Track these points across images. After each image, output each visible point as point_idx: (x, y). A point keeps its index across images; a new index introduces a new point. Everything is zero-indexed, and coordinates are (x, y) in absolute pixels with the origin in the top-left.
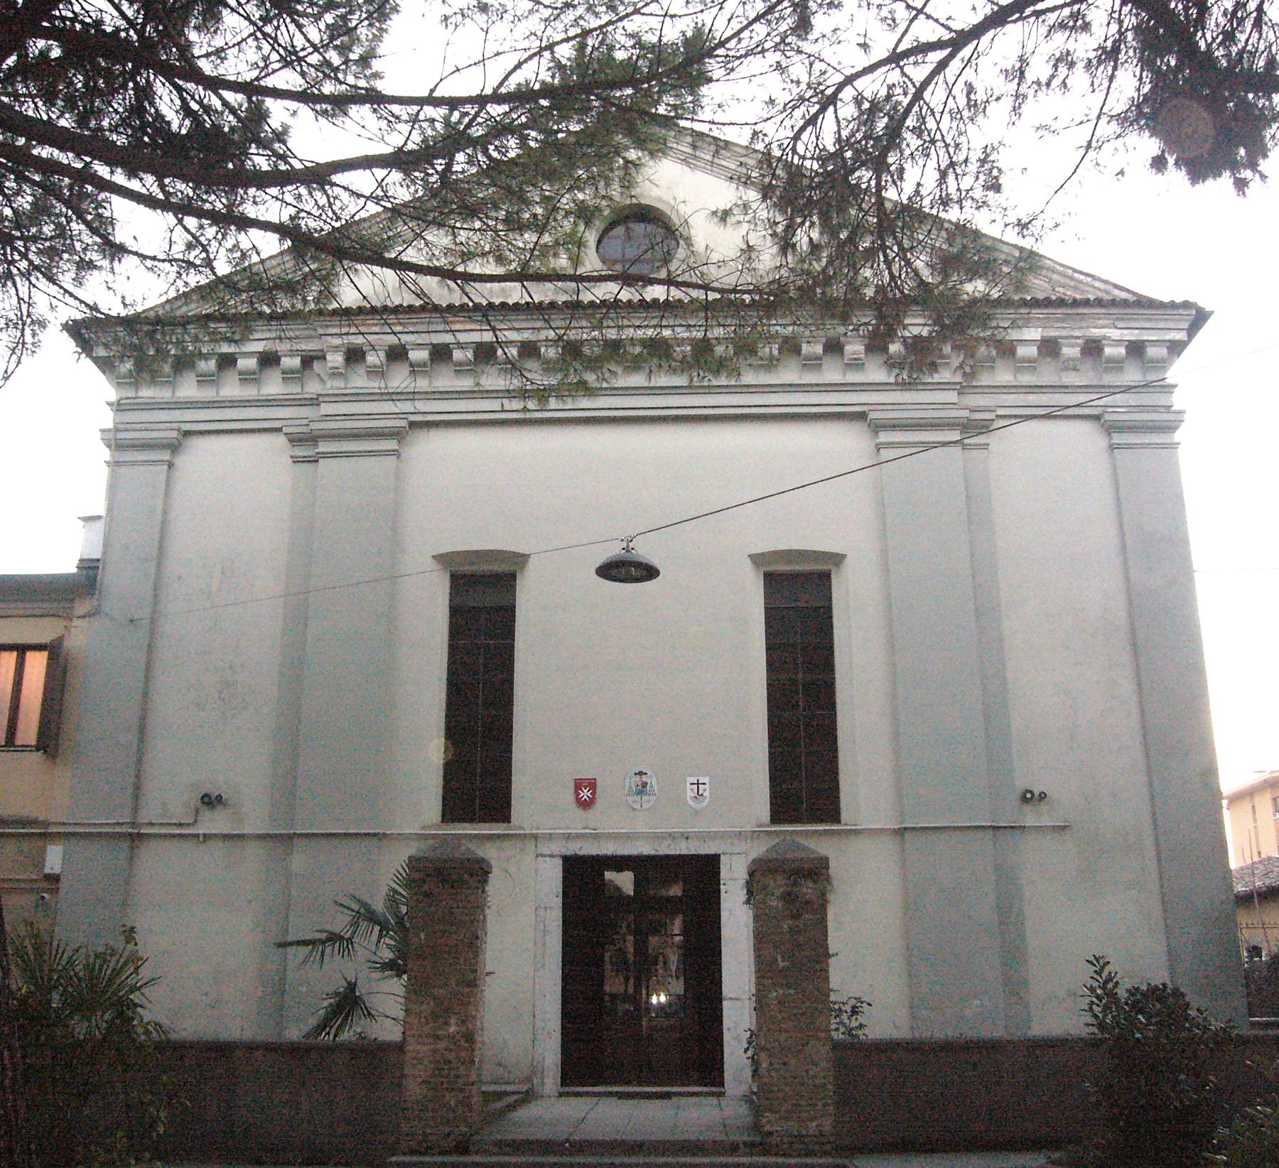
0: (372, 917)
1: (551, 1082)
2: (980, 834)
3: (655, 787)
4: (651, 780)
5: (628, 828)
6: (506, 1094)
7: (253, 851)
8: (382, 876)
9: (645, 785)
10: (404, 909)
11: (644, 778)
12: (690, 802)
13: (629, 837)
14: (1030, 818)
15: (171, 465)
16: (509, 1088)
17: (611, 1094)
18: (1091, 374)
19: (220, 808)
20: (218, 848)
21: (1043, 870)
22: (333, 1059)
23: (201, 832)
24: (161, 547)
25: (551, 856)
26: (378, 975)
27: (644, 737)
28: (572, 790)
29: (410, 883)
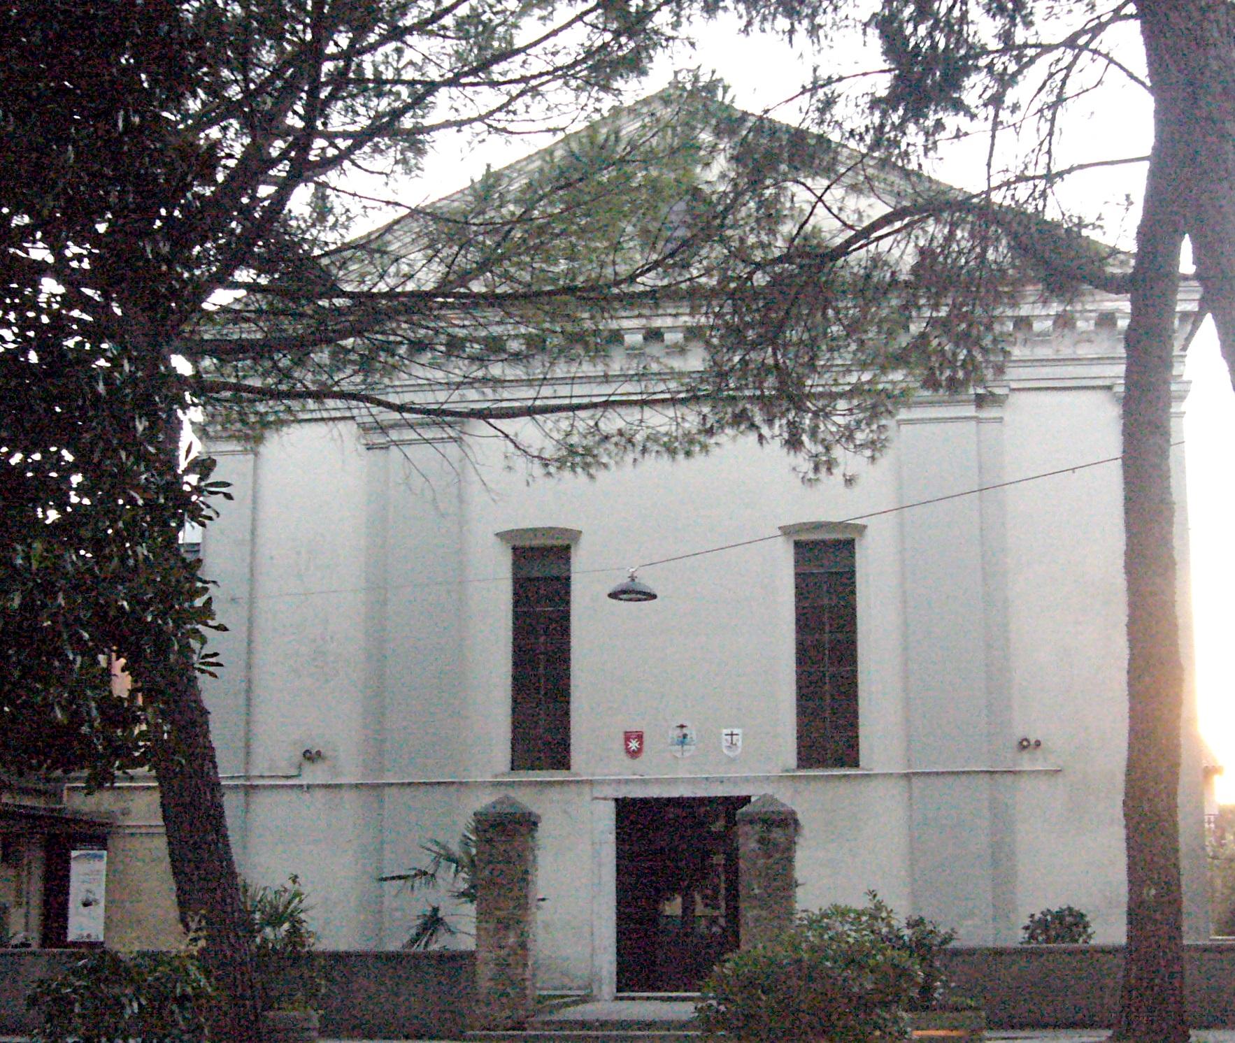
0: (450, 859)
1: (608, 986)
2: (981, 776)
3: (694, 737)
4: (691, 732)
5: (672, 776)
6: (568, 996)
7: (348, 795)
8: (455, 823)
9: (685, 736)
10: (474, 851)
11: (685, 731)
12: (725, 751)
13: (672, 782)
14: (1025, 763)
15: (256, 454)
16: (570, 993)
17: (656, 999)
18: (1106, 344)
19: (320, 761)
20: (319, 794)
21: (1035, 805)
22: (425, 966)
23: (304, 783)
24: (253, 532)
25: (605, 799)
26: (457, 901)
27: (687, 694)
28: (622, 741)
29: (476, 830)
